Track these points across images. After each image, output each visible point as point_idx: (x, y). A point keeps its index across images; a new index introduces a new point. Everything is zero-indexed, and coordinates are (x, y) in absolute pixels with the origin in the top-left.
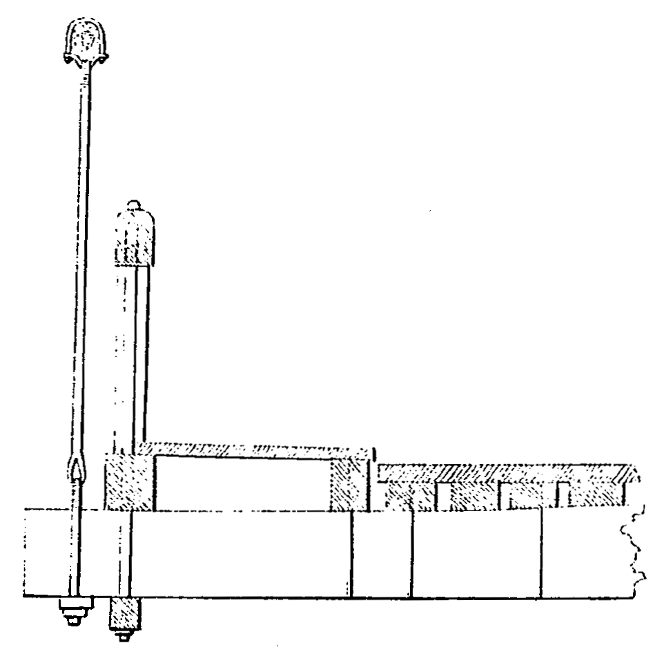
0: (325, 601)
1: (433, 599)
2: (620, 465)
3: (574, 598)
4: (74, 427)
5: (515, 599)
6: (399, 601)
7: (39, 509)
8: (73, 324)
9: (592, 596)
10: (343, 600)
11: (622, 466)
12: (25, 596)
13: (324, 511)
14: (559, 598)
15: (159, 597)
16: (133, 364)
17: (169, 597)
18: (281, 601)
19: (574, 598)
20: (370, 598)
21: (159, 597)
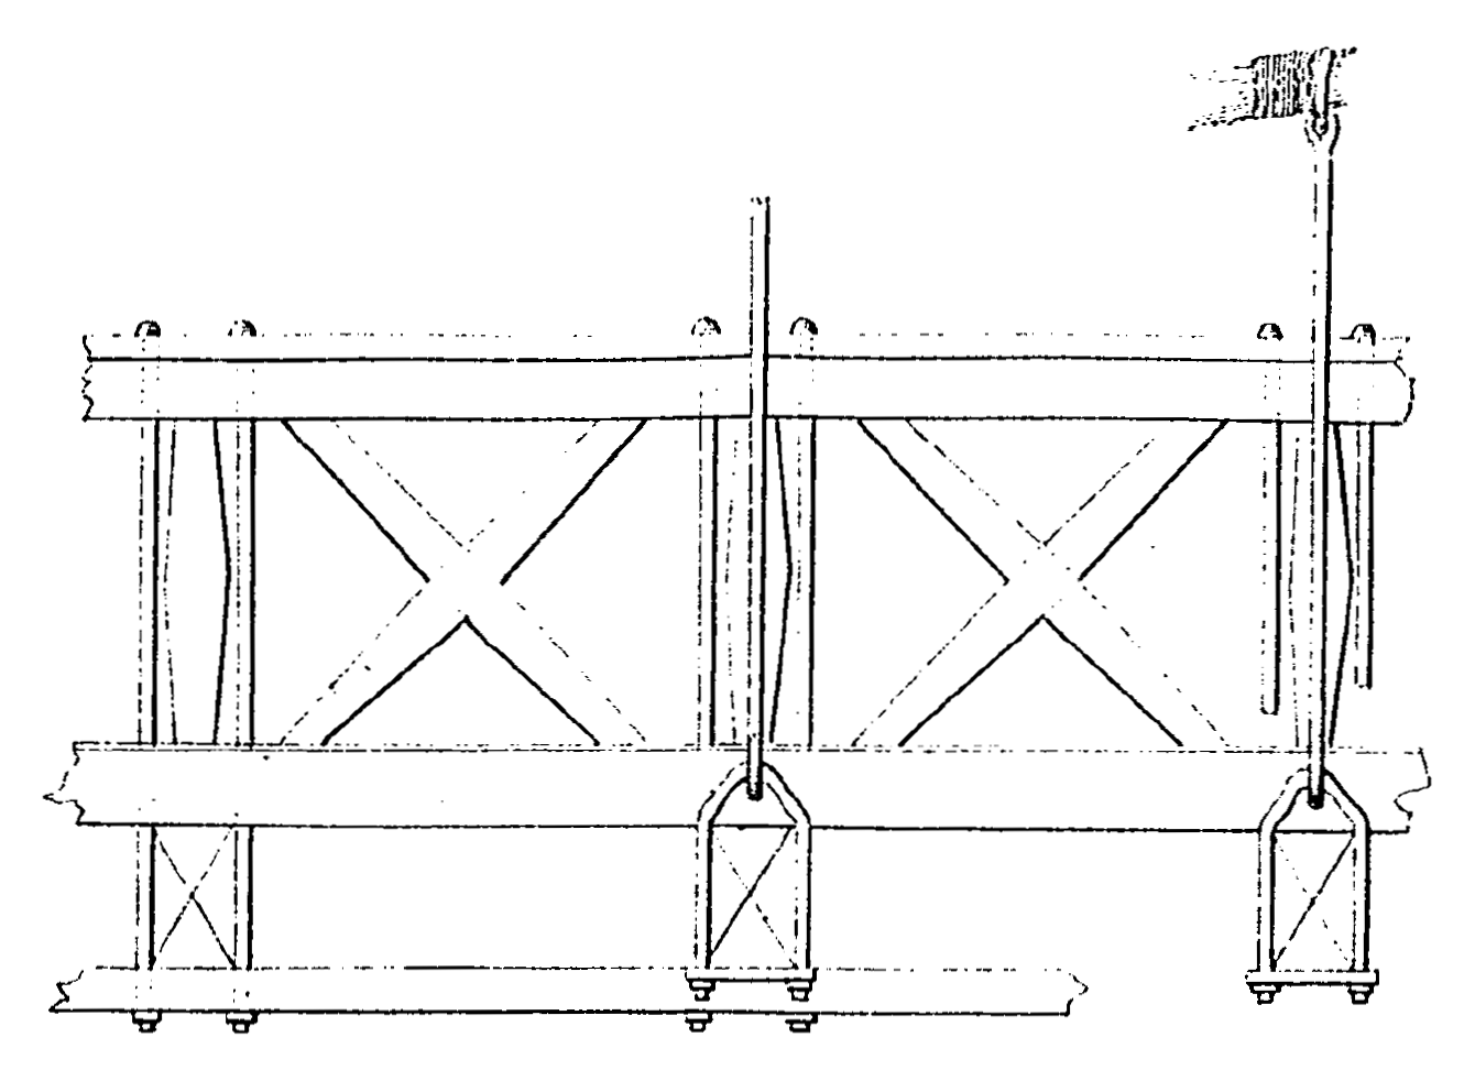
0: (815, 607)
1: (1161, 491)
2: (781, 827)
3: (1294, 362)
4: (921, 827)
5: (407, 419)
6: (305, 1014)
7: (299, 827)
8: (1389, 836)
9: (356, 1015)
10: (1332, 303)
11: (785, 830)
12: (1007, 580)
13: (540, 826)
14: (470, 420)
15: (1116, 359)
16: (966, 832)
17: (1133, 359)
18: (362, 355)
19: (1294, 362)
20: (301, 1012)
21: (1116, 359)
